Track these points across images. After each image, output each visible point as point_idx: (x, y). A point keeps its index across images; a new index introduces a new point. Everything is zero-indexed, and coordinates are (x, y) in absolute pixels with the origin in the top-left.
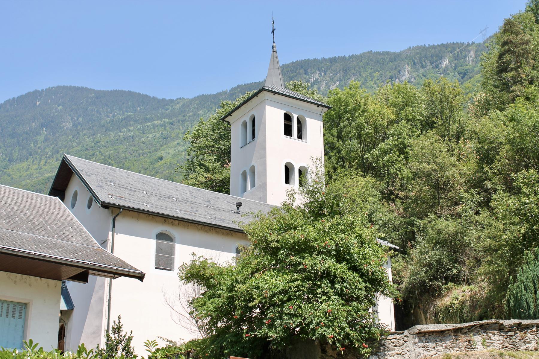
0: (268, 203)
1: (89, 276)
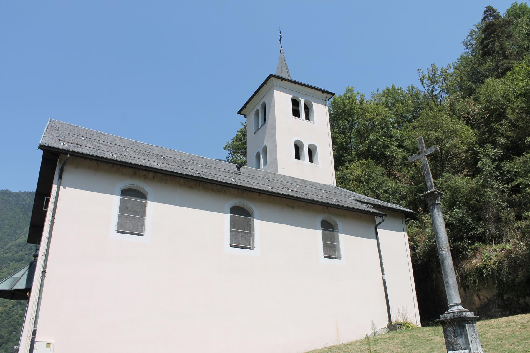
1: (460, 302)
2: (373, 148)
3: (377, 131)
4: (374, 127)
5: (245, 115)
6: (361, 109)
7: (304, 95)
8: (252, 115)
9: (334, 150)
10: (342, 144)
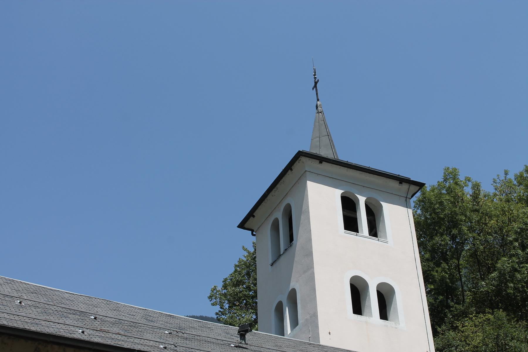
0: (321, 344)
2: (508, 287)
3: (513, 252)
4: (504, 244)
5: (252, 231)
6: (477, 211)
7: (364, 188)
8: (267, 231)
9: (428, 293)
10: (443, 278)
